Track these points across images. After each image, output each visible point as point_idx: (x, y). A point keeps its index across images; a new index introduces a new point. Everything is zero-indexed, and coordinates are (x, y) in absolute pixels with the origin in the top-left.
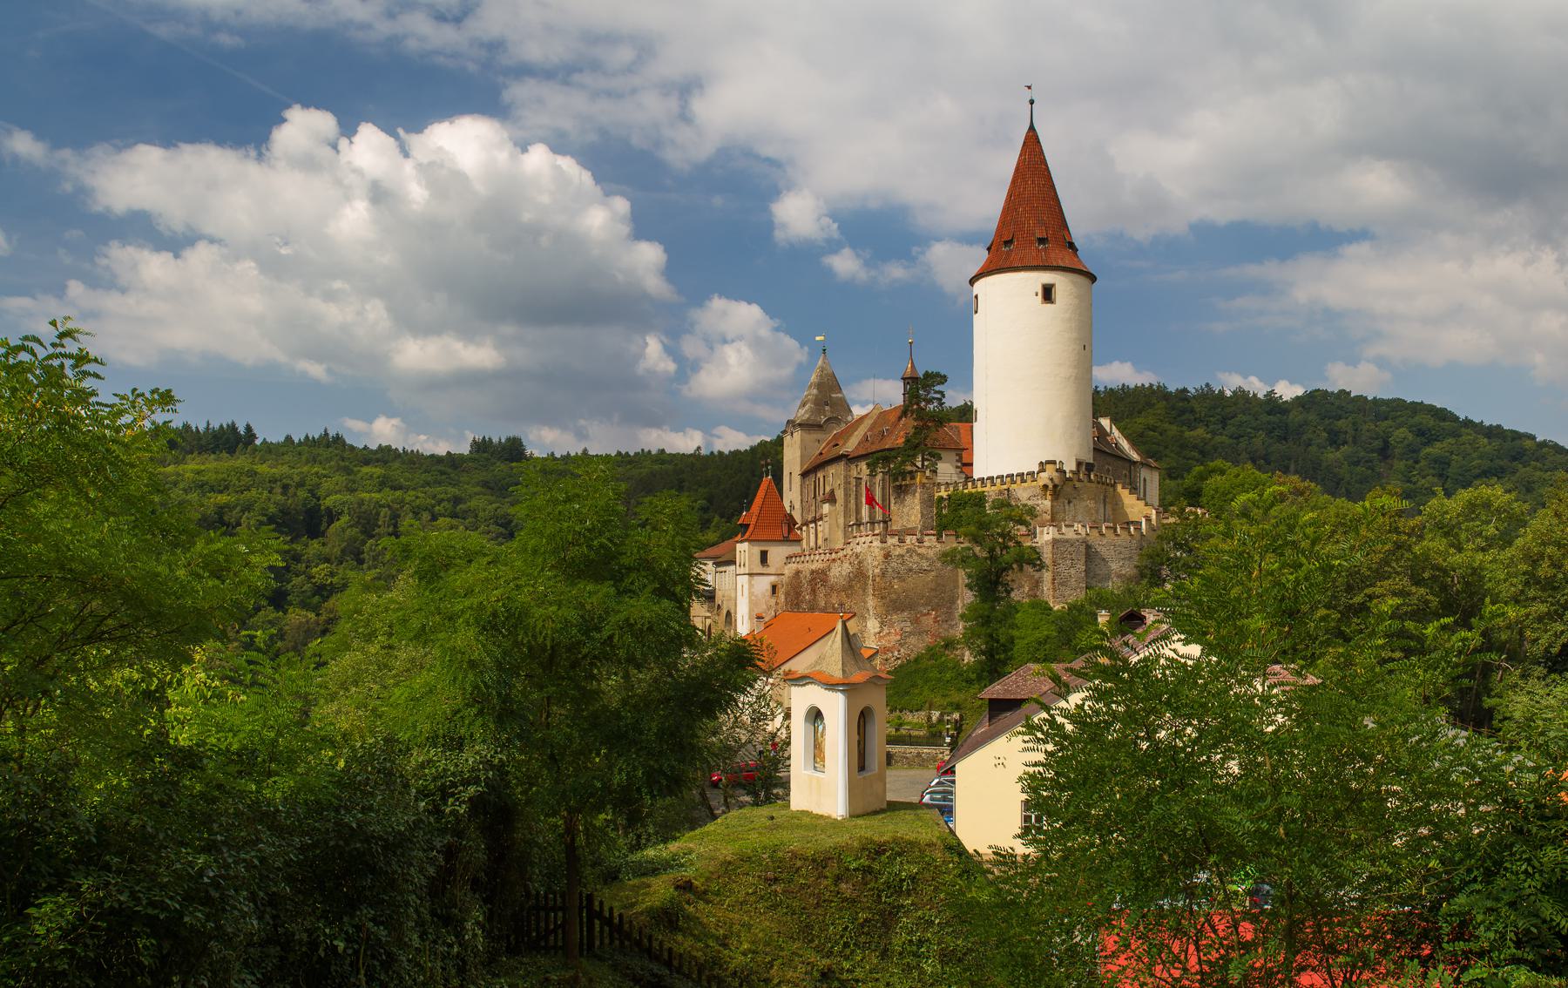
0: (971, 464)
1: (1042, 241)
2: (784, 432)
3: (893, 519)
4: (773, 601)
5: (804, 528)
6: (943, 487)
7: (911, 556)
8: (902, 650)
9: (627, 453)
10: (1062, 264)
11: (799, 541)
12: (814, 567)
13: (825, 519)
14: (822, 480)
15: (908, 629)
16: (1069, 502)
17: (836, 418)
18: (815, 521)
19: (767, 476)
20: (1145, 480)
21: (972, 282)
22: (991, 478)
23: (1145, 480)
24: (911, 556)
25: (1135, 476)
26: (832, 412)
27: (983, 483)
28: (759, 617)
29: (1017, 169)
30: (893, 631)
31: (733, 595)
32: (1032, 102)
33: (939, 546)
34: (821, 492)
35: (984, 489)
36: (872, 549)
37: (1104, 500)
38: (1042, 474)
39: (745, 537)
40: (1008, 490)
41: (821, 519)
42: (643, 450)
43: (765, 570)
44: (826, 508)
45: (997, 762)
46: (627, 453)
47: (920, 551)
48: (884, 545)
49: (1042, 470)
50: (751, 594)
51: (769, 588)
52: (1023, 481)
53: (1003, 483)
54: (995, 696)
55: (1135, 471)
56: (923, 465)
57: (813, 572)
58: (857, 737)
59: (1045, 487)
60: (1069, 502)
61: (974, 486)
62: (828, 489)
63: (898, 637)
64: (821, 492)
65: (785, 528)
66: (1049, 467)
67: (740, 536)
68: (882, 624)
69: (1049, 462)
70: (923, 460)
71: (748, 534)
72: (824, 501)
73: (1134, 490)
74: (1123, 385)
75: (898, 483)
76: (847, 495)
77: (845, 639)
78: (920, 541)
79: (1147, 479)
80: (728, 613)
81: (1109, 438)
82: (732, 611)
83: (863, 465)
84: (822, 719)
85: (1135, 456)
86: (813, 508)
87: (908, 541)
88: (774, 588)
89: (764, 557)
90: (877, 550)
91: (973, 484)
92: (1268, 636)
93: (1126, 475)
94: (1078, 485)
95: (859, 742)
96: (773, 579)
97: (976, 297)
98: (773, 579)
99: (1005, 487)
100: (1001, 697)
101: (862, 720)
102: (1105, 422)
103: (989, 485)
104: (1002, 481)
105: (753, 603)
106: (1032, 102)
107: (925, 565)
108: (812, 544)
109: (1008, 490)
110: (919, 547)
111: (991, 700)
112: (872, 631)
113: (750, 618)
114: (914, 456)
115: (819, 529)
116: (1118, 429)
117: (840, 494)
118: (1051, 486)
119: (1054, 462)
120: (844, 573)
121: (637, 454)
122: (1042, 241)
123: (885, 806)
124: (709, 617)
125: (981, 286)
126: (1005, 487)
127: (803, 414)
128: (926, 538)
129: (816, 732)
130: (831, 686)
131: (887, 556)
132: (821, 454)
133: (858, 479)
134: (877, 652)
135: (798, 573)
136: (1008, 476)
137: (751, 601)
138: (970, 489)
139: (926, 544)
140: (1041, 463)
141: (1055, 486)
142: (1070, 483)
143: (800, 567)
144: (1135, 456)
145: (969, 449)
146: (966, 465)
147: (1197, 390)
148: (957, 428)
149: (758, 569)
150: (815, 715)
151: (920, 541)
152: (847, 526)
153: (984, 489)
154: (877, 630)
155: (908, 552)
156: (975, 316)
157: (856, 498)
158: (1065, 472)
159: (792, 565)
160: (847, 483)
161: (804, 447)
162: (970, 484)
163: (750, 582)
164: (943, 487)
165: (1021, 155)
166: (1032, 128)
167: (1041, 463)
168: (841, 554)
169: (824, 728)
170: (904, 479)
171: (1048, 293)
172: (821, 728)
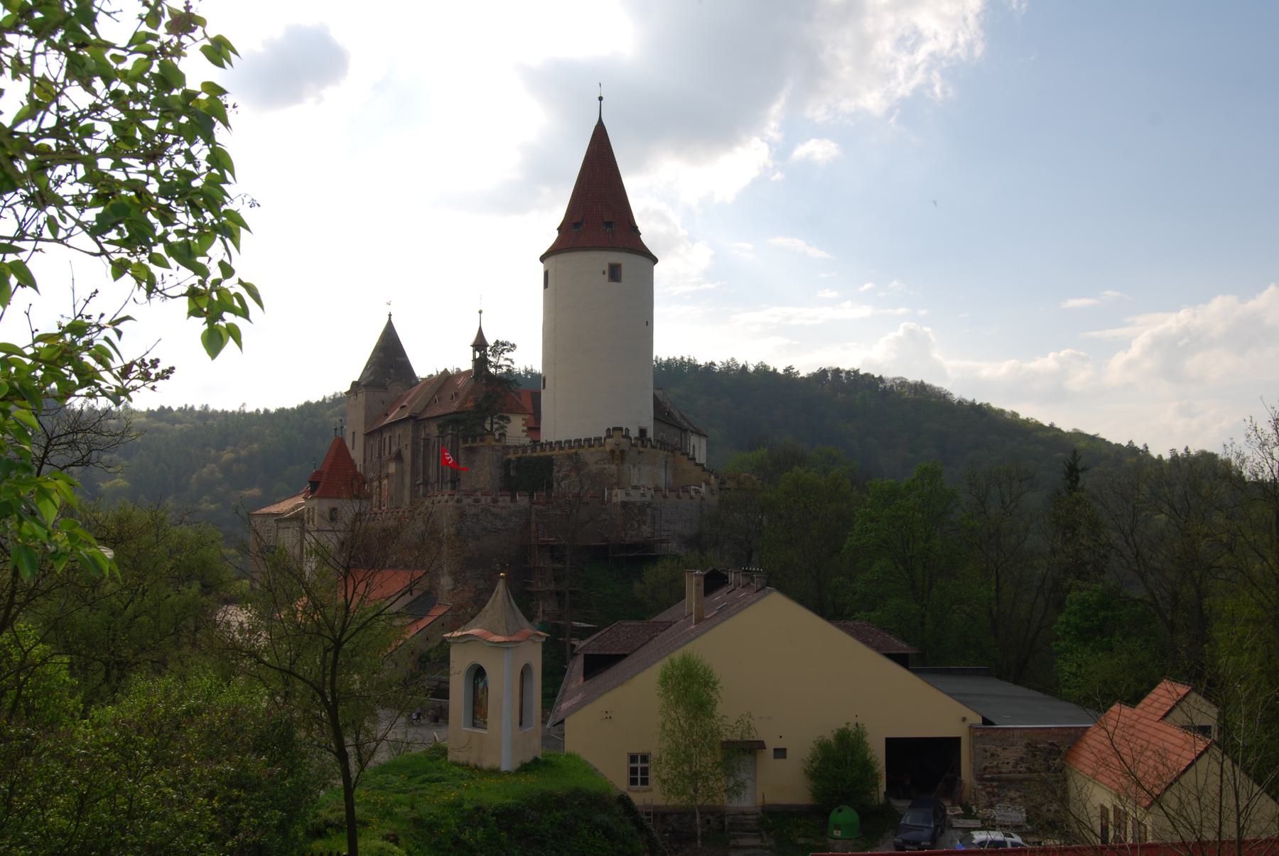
1: (609, 224)
6: (511, 451)
14: (387, 440)
15: (481, 587)
16: (634, 466)
20: (694, 447)
22: (559, 443)
23: (694, 447)
27: (551, 447)
33: (512, 505)
34: (387, 452)
35: (553, 453)
37: (666, 465)
38: (608, 440)
39: (315, 494)
40: (576, 454)
42: (186, 405)
44: (392, 468)
46: (170, 408)
47: (494, 510)
49: (609, 436)
52: (591, 446)
53: (571, 447)
56: (492, 427)
60: (634, 466)
61: (543, 450)
62: (394, 449)
63: (472, 594)
64: (387, 452)
68: (456, 581)
69: (615, 429)
70: (492, 424)
72: (390, 460)
75: (468, 445)
78: (495, 501)
79: (697, 445)
87: (483, 502)
91: (542, 447)
92: (282, 590)
94: (641, 449)
99: (573, 451)
100: (596, 653)
103: (557, 449)
106: (601, 99)
109: (576, 454)
110: (494, 507)
112: (447, 588)
114: (484, 419)
117: (407, 454)
118: (617, 452)
119: (621, 429)
121: (180, 410)
122: (609, 224)
126: (573, 451)
128: (500, 499)
129: (475, 687)
131: (462, 515)
133: (427, 440)
136: (566, 442)
138: (538, 453)
139: (500, 504)
147: (723, 364)
151: (495, 501)
152: (413, 485)
153: (553, 453)
154: (451, 587)
155: (483, 511)
157: (424, 459)
160: (415, 443)
162: (538, 448)
164: (511, 451)
167: (609, 429)
169: (486, 684)
172: (481, 685)
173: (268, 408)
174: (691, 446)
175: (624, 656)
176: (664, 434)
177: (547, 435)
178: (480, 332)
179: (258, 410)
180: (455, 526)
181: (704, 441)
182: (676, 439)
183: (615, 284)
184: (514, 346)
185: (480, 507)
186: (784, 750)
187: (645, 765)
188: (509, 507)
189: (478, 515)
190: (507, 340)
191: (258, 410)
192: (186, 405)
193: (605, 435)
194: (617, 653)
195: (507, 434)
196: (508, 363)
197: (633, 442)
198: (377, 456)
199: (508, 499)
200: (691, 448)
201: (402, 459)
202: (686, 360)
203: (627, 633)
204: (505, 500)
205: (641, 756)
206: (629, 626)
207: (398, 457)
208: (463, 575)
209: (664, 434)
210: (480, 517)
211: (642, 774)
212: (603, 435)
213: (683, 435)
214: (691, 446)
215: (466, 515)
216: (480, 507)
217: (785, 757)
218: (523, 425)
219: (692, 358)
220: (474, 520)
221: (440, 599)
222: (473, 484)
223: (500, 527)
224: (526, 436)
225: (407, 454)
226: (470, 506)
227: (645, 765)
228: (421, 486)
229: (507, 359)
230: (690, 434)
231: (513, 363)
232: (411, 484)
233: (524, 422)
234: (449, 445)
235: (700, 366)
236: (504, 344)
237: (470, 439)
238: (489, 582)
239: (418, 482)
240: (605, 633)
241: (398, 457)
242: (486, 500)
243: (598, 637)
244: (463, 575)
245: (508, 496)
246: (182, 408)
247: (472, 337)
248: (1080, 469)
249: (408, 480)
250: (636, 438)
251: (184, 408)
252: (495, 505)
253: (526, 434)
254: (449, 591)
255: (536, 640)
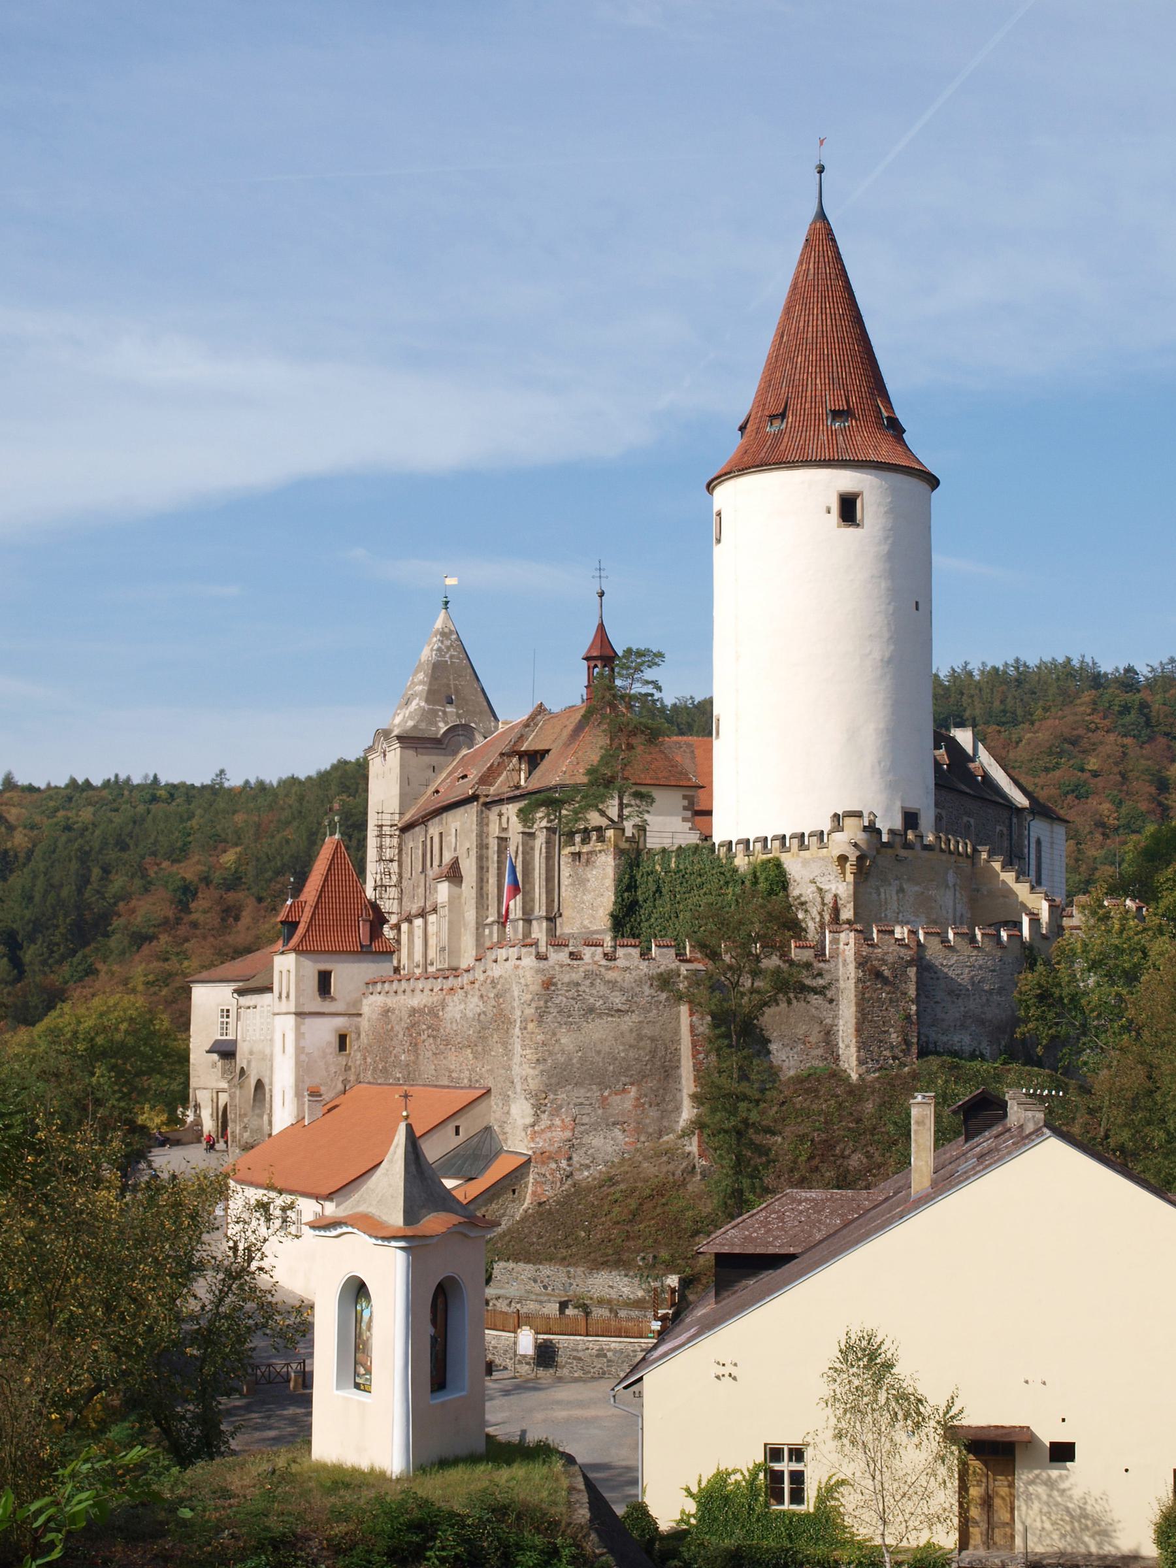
0: (709, 813)
1: (836, 414)
2: (370, 749)
3: (565, 913)
4: (342, 1060)
5: (404, 927)
7: (592, 984)
8: (575, 1158)
9: (87, 782)
10: (873, 458)
11: (388, 953)
12: (416, 1001)
13: (441, 911)
17: (466, 727)
18: (423, 914)
19: (332, 834)
21: (710, 487)
23: (1039, 842)
24: (592, 984)
25: (1020, 835)
26: (459, 716)
28: (315, 1093)
29: (794, 287)
30: (557, 1122)
31: (267, 1051)
32: (821, 169)
33: (644, 965)
34: (436, 863)
36: (520, 972)
38: (837, 836)
41: (435, 910)
42: (117, 776)
43: (328, 1007)
44: (443, 890)
45: (721, 1371)
46: (87, 782)
47: (610, 975)
48: (543, 964)
50: (299, 1050)
51: (334, 1041)
52: (802, 846)
54: (726, 1250)
55: (1020, 825)
57: (413, 1011)
58: (430, 1330)
59: (842, 859)
62: (448, 857)
63: (568, 1134)
64: (436, 863)
65: (364, 930)
66: (849, 822)
67: (280, 942)
68: (539, 1108)
70: (621, 806)
71: (295, 940)
72: (438, 879)
73: (1014, 858)
74: (1017, 660)
76: (482, 869)
77: (412, 1157)
80: (259, 1085)
81: (971, 765)
82: (266, 1081)
83: (511, 810)
84: (367, 1296)
85: (1021, 800)
86: (421, 890)
87: (587, 957)
88: (342, 1040)
89: (324, 982)
90: (528, 974)
93: (1001, 834)
94: (903, 853)
95: (434, 1340)
96: (340, 1022)
97: (719, 514)
98: (340, 1022)
101: (440, 1300)
102: (964, 737)
104: (765, 846)
105: (303, 1067)
106: (821, 169)
107: (618, 1000)
108: (418, 956)
110: (608, 968)
111: (718, 1256)
113: (298, 1094)
115: (432, 929)
116: (988, 748)
117: (469, 868)
118: (853, 858)
119: (858, 815)
120: (470, 1015)
122: (836, 414)
123: (481, 1447)
124: (224, 1091)
125: (727, 495)
127: (402, 720)
128: (620, 952)
130: (385, 1235)
132: (437, 792)
134: (529, 1161)
135: (386, 1012)
136: (774, 838)
137: (298, 1063)
139: (620, 963)
140: (836, 816)
141: (861, 859)
142: (889, 851)
143: (391, 1001)
144: (1021, 800)
145: (705, 787)
146: (701, 813)
147: (1153, 670)
148: (689, 745)
149: (316, 1004)
150: (357, 1290)
152: (480, 925)
155: (586, 977)
156: (717, 549)
158: (879, 832)
159: (372, 998)
160: (482, 846)
161: (406, 780)
163: (297, 1028)
165: (801, 263)
166: (821, 216)
168: (465, 979)
170: (585, 841)
171: (848, 509)
173: (262, 777)
174: (1033, 840)
175: (790, 1257)
176: (972, 821)
177: (723, 830)
178: (601, 628)
179: (247, 782)
180: (533, 1005)
181: (1060, 830)
182: (998, 828)
183: (851, 531)
184: (660, 655)
185: (582, 969)
186: (1071, 1446)
187: (795, 1466)
188: (637, 968)
189: (578, 984)
190: (647, 647)
191: (247, 782)
192: (117, 776)
193: (829, 828)
194: (777, 1251)
195: (648, 828)
196: (649, 689)
197: (885, 838)
198: (420, 870)
199: (635, 952)
200: (1033, 845)
201: (462, 877)
202: (1076, 663)
203: (801, 1212)
204: (628, 956)
205: (790, 1450)
206: (806, 1200)
207: (454, 874)
208: (551, 1096)
209: (972, 821)
210: (581, 988)
211: (792, 1482)
212: (826, 826)
213: (1015, 820)
214: (1033, 840)
215: (555, 984)
216: (582, 969)
217: (1071, 1458)
218: (685, 808)
219: (1088, 660)
220: (569, 994)
221: (509, 1142)
222: (586, 922)
223: (620, 1006)
224: (690, 829)
225: (469, 868)
226: (562, 966)
227: (795, 1466)
228: (495, 927)
229: (647, 682)
230: (1029, 819)
231: (659, 689)
232: (477, 923)
233: (686, 803)
234: (544, 850)
235: (1106, 674)
236: (640, 654)
237: (578, 838)
238: (600, 1112)
239: (490, 920)
240: (758, 1213)
241: (454, 874)
242: (593, 955)
243: (744, 1221)
244: (551, 1096)
245: (635, 946)
246: (109, 780)
247: (585, 640)
248: (829, 996)
249: (470, 915)
250: (891, 832)
251: (113, 779)
252: (611, 964)
253: (689, 825)
254: (525, 1128)
255: (472, 1235)
